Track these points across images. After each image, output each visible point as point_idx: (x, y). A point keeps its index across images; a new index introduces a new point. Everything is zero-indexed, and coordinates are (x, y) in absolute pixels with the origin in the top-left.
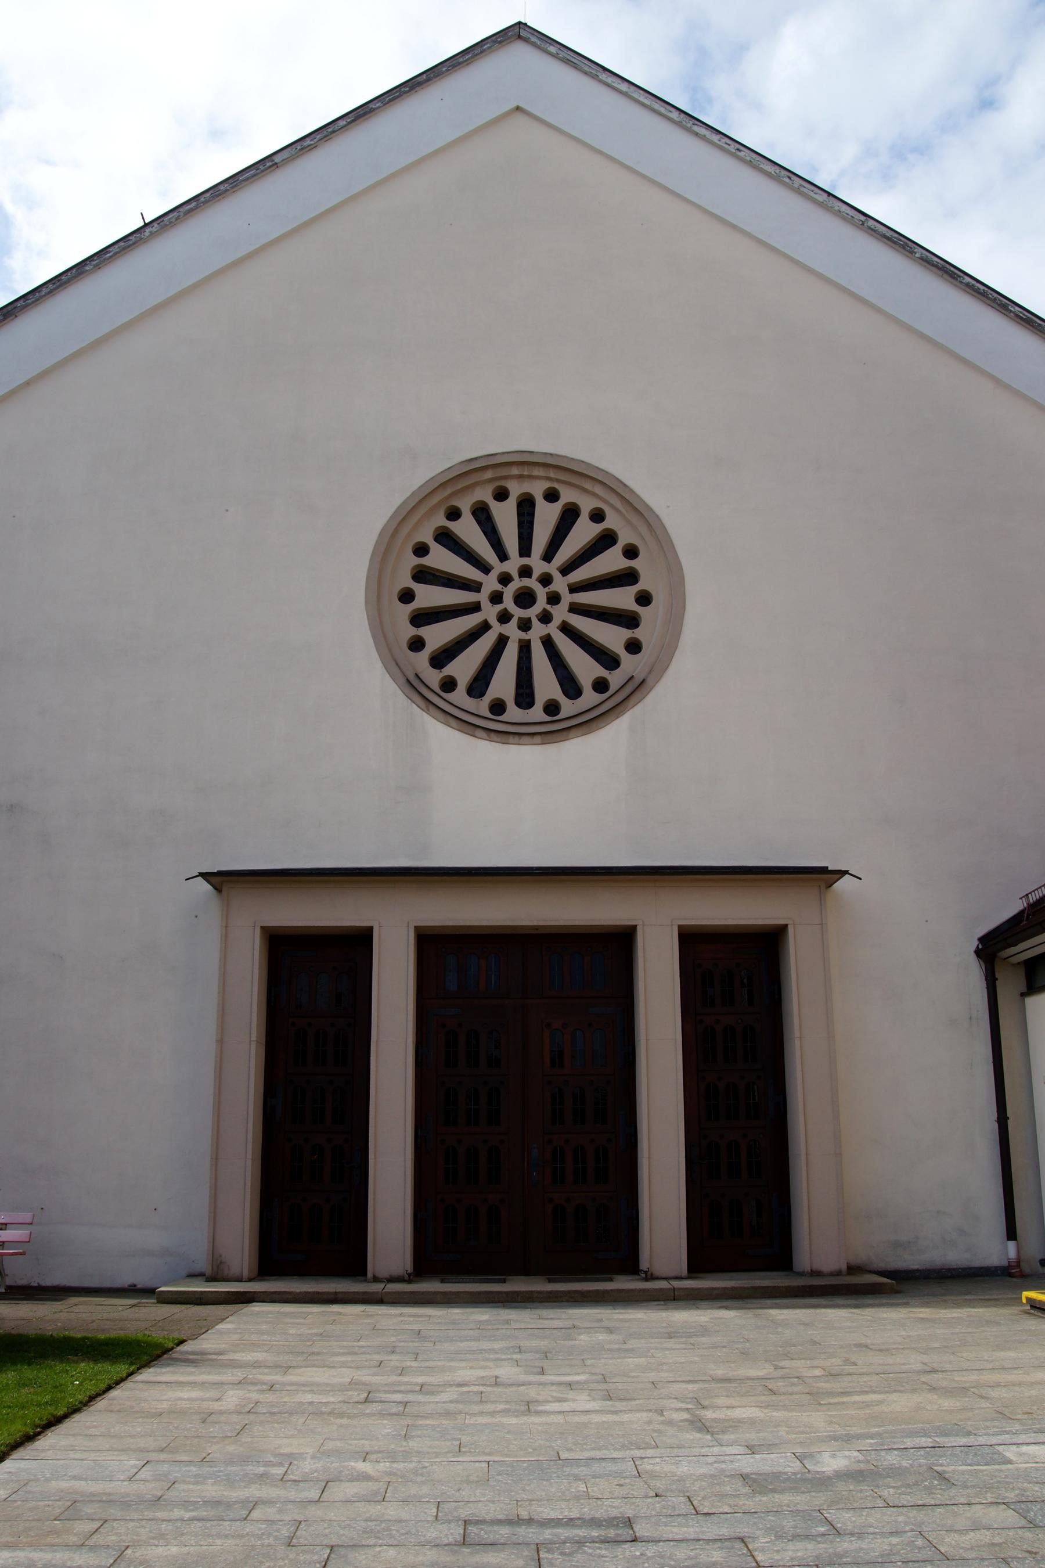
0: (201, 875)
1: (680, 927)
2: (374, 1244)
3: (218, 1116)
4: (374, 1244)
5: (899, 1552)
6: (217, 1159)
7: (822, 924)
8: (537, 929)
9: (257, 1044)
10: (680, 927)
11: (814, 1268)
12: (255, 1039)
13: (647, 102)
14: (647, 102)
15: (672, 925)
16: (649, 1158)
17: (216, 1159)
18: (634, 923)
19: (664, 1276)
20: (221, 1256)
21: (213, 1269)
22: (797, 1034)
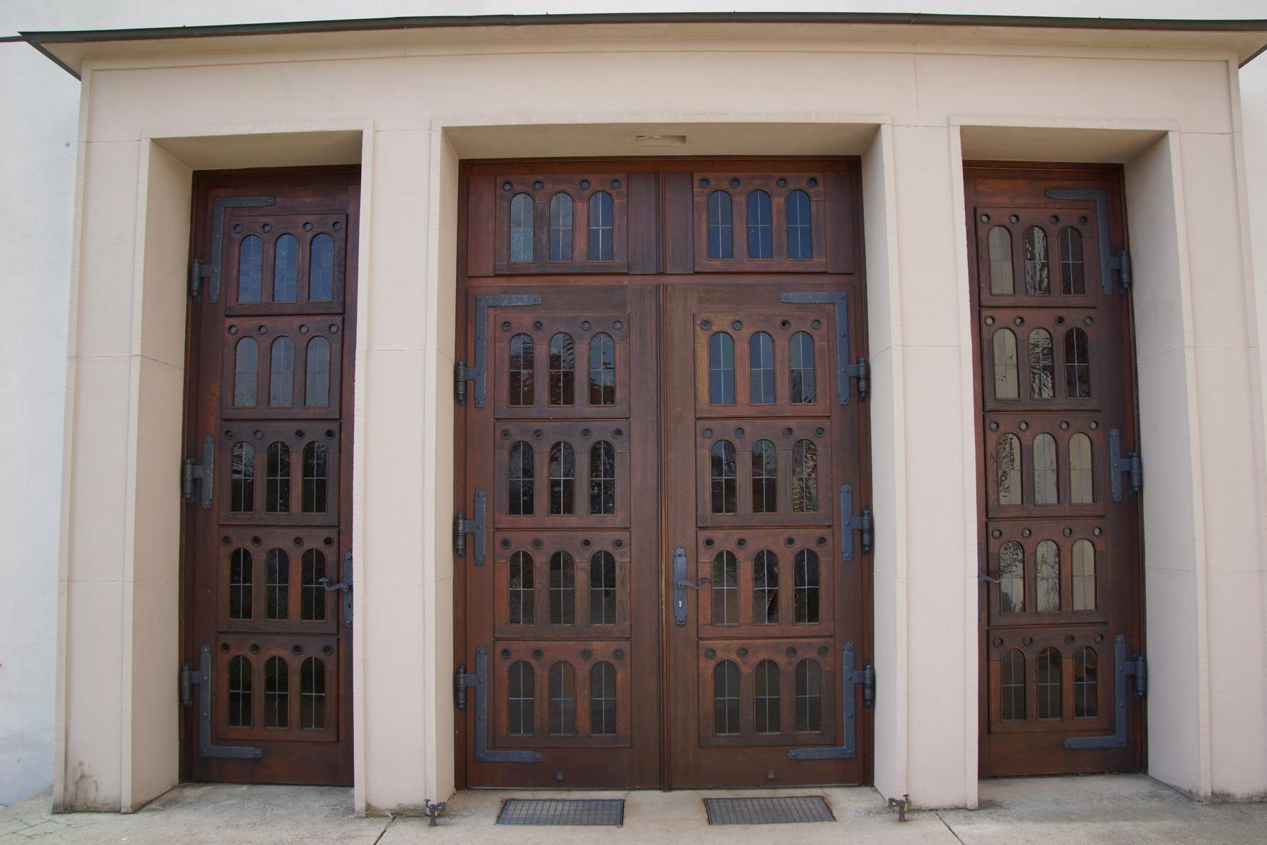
0: (27, 37)
1: (963, 129)
2: (366, 736)
3: (83, 233)
4: (366, 736)
5: (526, 817)
6: (70, 581)
7: (1232, 133)
8: (683, 139)
9: (142, 362)
10: (963, 129)
11: (1216, 791)
12: (138, 352)
13: (279, 29)
14: (279, 29)
15: (949, 126)
16: (907, 579)
17: (69, 582)
18: (874, 121)
19: (933, 804)
20: (81, 764)
21: (66, 788)
22: (1188, 339)
